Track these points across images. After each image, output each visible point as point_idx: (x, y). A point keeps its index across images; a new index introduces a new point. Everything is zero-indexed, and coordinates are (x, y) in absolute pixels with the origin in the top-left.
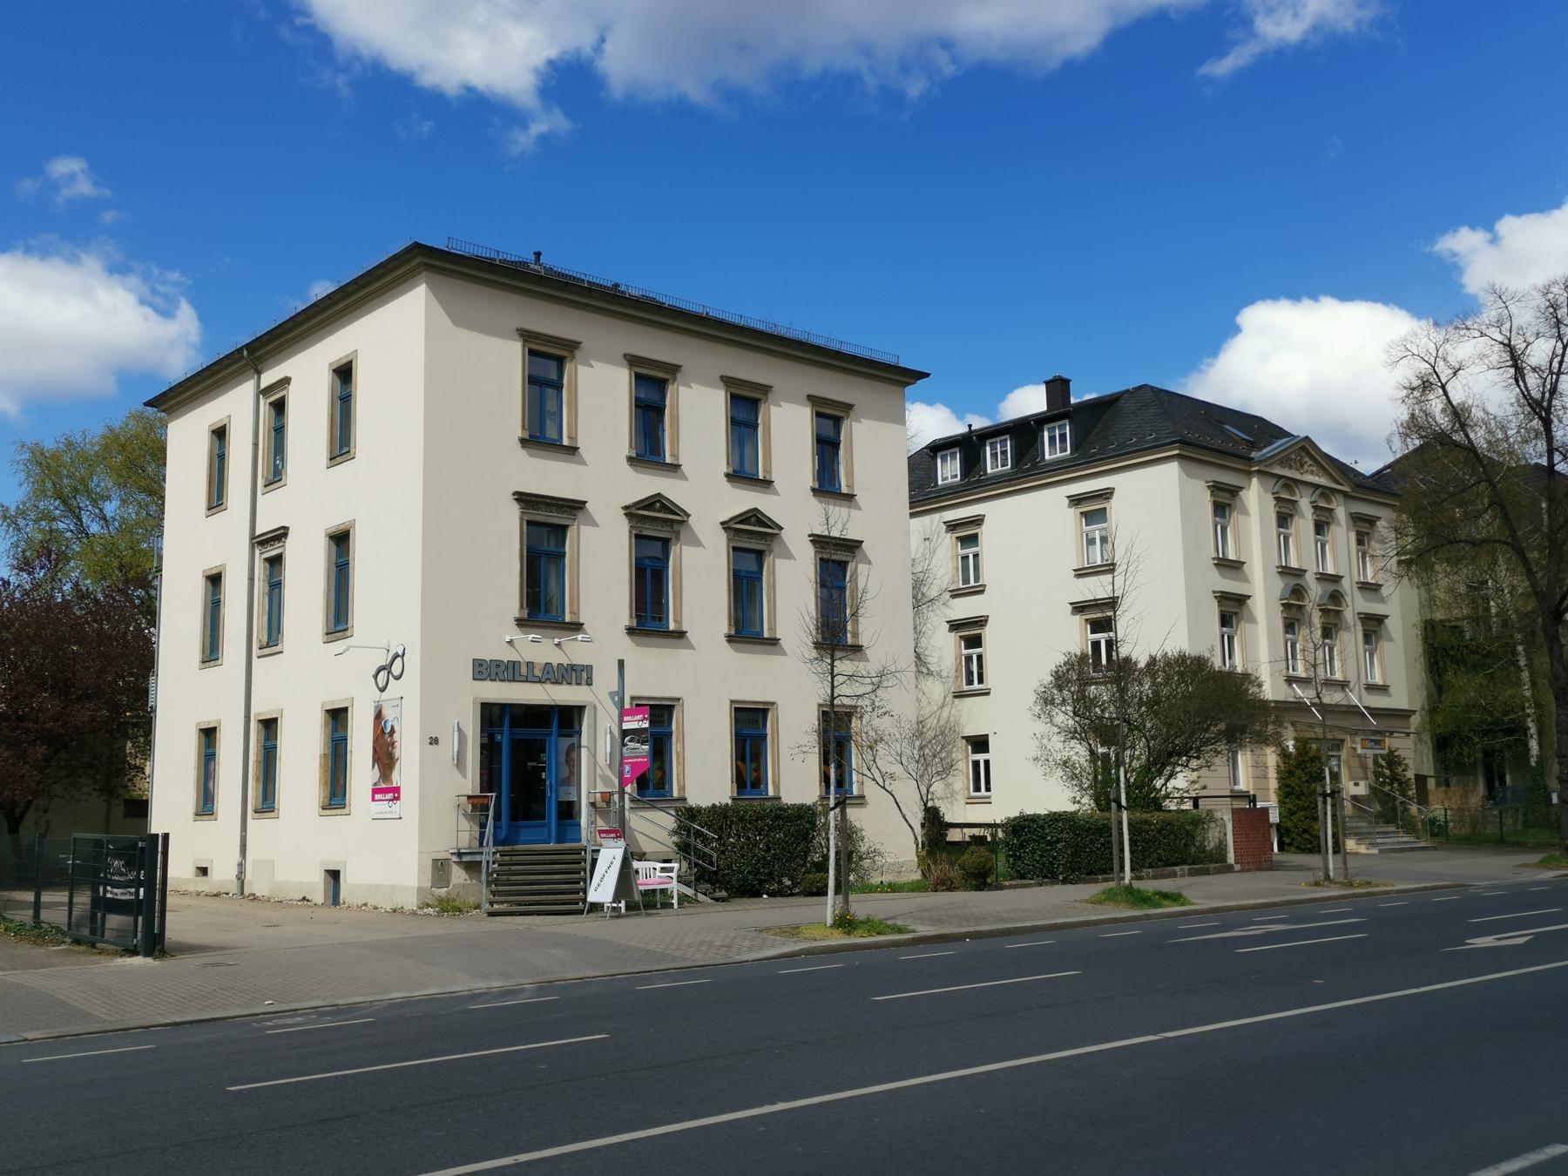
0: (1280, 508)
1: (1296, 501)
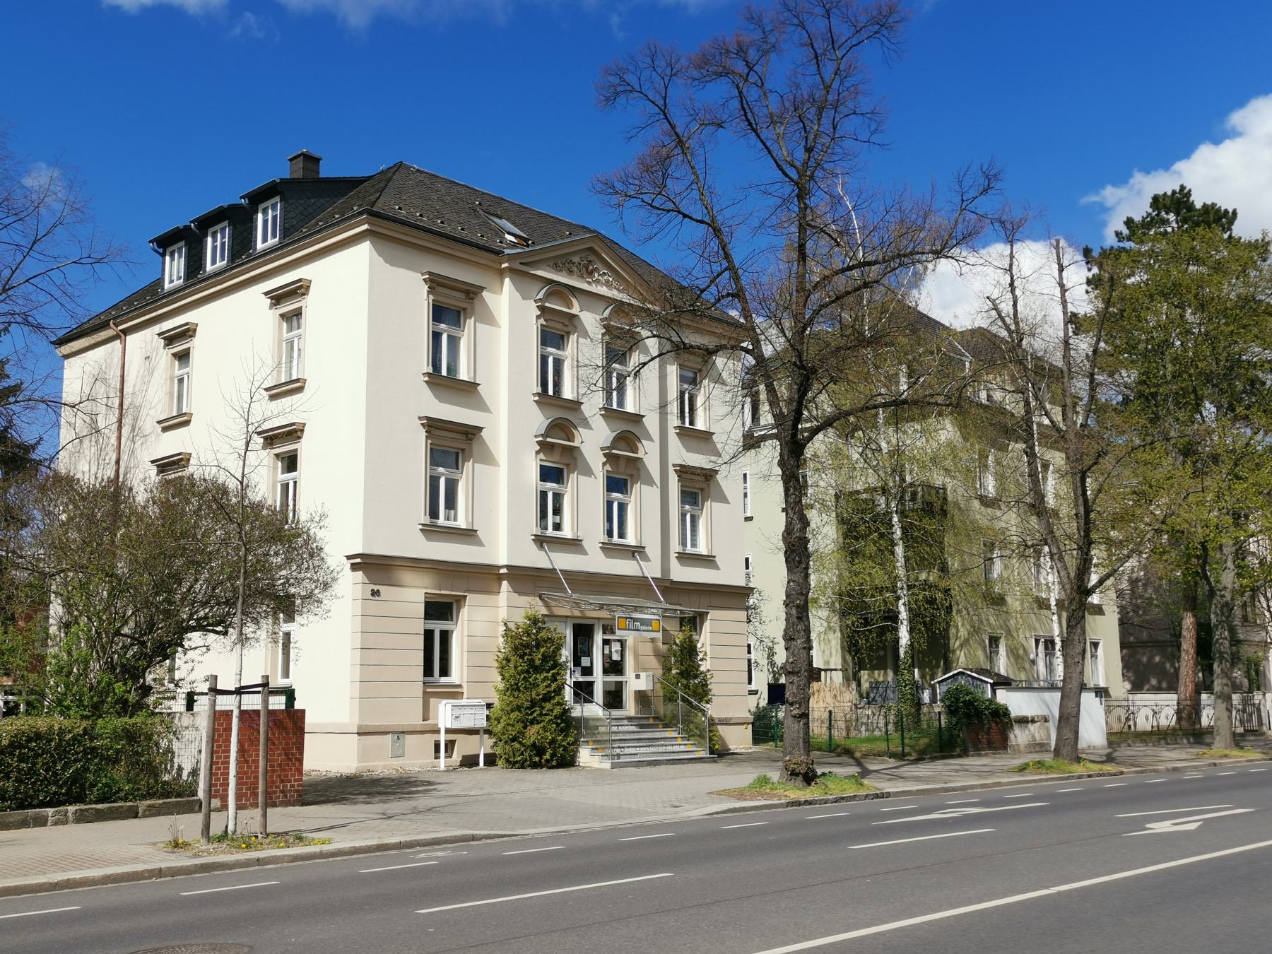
0: (546, 320)
1: (574, 316)
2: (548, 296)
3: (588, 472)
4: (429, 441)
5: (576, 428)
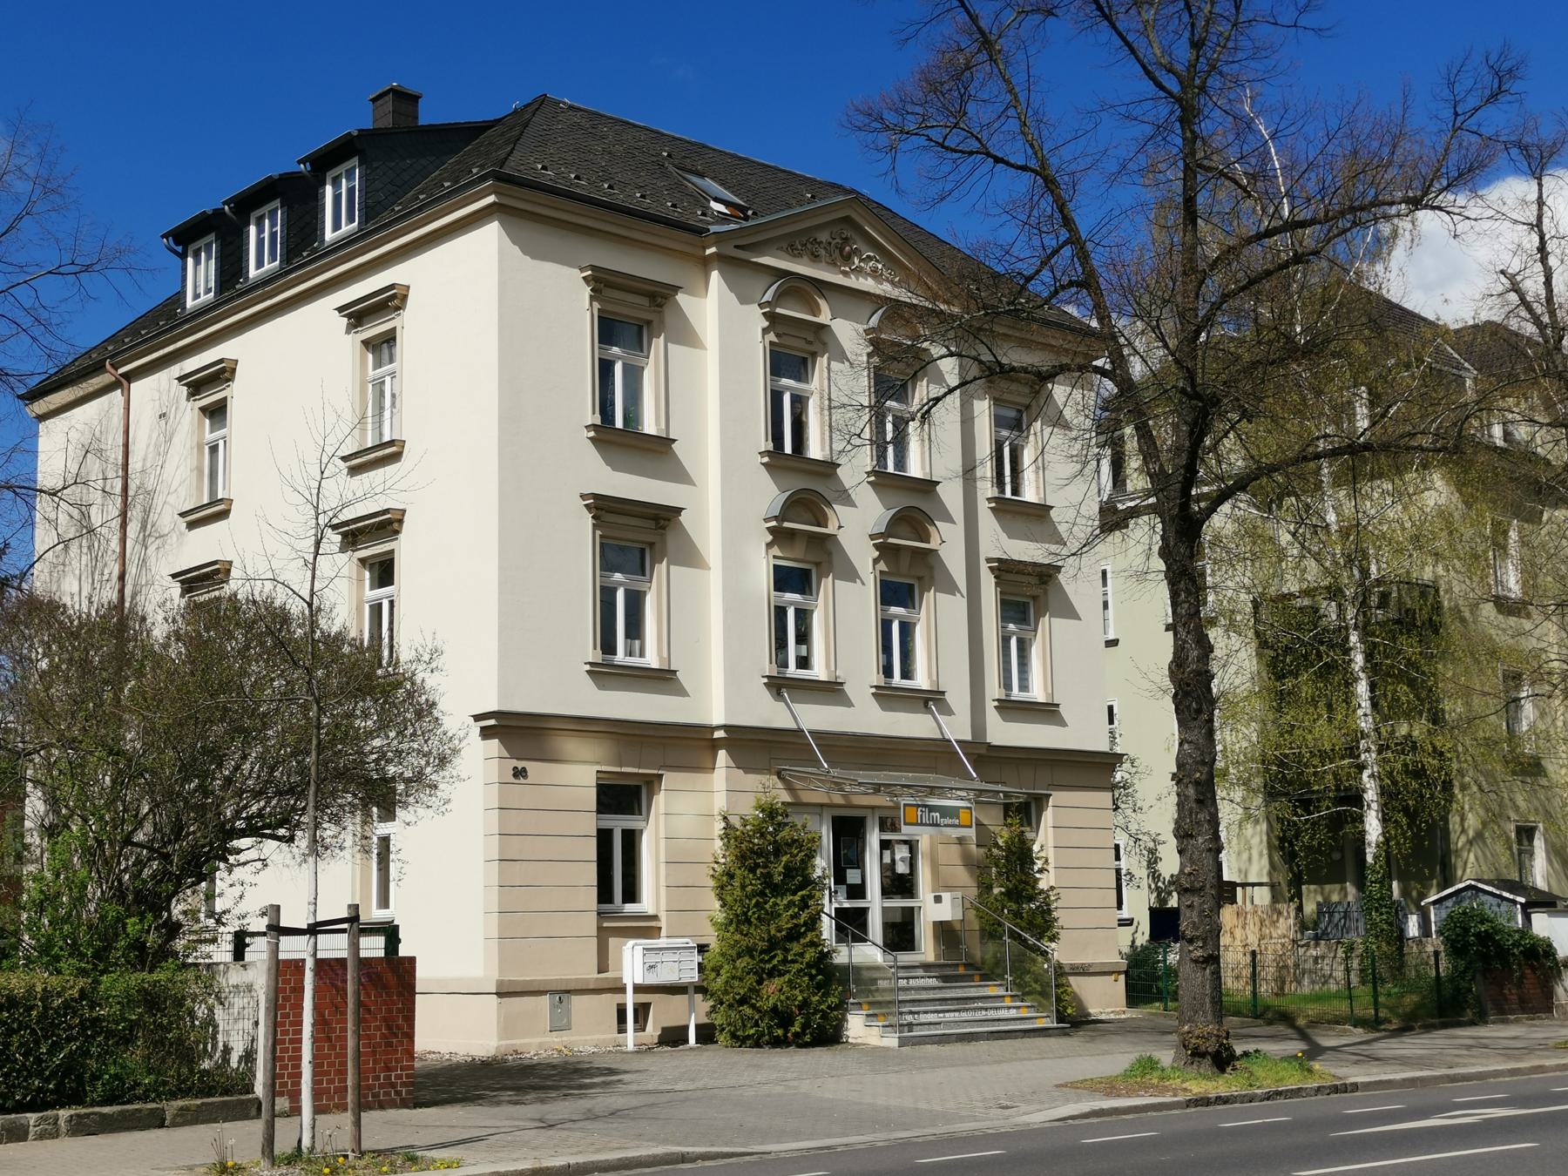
2: (780, 297)
3: (851, 574)
4: (598, 533)
5: (829, 505)
